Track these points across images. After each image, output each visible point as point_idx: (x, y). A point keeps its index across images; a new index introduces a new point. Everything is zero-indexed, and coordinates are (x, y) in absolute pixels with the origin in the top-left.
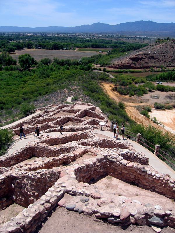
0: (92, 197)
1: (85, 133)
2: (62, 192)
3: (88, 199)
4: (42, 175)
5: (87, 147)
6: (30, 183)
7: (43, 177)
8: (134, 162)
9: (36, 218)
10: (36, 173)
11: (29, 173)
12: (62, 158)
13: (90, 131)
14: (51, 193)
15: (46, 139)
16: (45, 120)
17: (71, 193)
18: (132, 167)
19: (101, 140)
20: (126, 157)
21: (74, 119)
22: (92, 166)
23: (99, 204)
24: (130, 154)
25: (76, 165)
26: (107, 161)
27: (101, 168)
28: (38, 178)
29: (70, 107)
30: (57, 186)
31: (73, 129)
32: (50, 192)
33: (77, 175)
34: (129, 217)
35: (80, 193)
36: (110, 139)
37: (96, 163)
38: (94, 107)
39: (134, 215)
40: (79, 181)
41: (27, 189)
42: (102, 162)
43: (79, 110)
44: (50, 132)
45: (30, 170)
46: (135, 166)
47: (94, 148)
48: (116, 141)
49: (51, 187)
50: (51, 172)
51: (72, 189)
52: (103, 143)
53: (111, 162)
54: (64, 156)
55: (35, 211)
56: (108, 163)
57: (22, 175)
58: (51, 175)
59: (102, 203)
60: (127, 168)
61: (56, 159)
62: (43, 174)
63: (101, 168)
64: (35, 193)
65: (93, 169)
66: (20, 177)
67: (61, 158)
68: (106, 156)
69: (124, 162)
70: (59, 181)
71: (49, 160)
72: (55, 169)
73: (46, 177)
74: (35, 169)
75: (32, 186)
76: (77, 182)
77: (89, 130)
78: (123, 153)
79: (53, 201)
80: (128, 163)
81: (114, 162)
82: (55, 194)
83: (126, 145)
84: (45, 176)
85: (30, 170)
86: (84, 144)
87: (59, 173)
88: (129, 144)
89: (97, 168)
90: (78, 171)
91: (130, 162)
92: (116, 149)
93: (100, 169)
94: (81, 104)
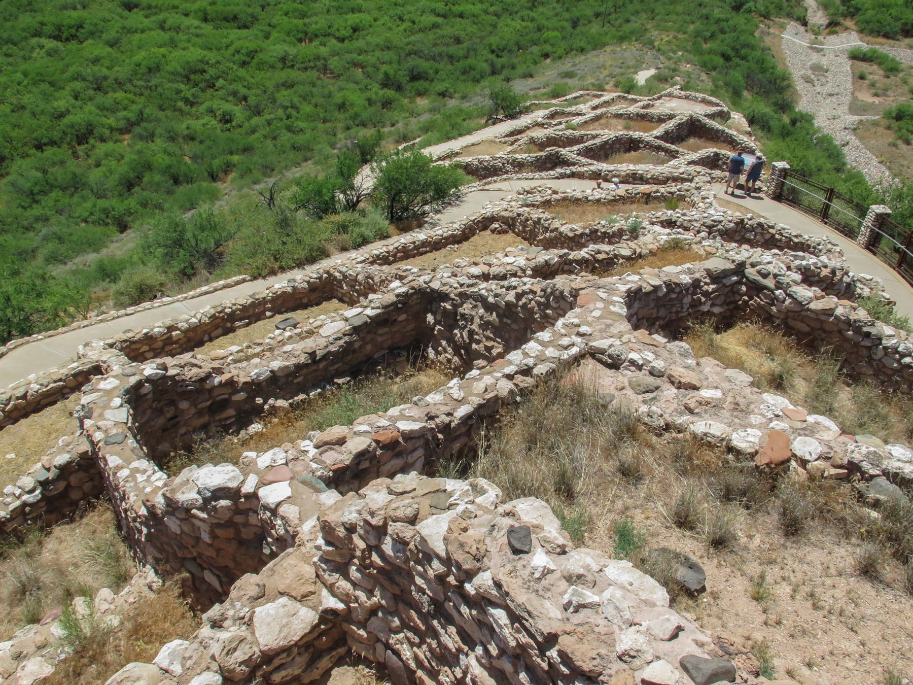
0: (672, 383)
1: (679, 191)
2: (574, 350)
3: (655, 385)
4: (519, 296)
5: (679, 233)
6: (481, 318)
7: (524, 300)
8: (839, 299)
9: (483, 412)
10: (502, 287)
11: (481, 287)
12: (590, 258)
13: (698, 188)
14: (540, 348)
15: (549, 197)
16: (551, 141)
17: (605, 358)
18: (829, 312)
19: (730, 218)
20: (809, 277)
21: (649, 146)
22: (687, 290)
23: (692, 406)
24: (828, 270)
25: (632, 280)
26: (739, 283)
27: (718, 302)
28: (508, 304)
29: (641, 104)
30: (563, 331)
31: (641, 175)
32: (536, 344)
33: (633, 311)
34: (788, 460)
35: (633, 363)
36: (762, 220)
37: (702, 284)
38: (726, 109)
39: (808, 461)
40: (636, 327)
41: (471, 333)
42: (724, 281)
43: (671, 117)
44: (562, 176)
45: (486, 277)
46: (839, 311)
47: (703, 239)
48: (784, 229)
49: (542, 329)
50: (549, 290)
51: (610, 346)
52: (736, 231)
53: (756, 288)
54: (599, 252)
55: (486, 390)
56: (744, 288)
57: (460, 290)
58: (548, 299)
59: (700, 404)
60: (812, 315)
61: (571, 257)
62: (524, 293)
63: (718, 302)
64: (492, 347)
65: (687, 300)
66: (452, 296)
67: (587, 256)
68: (742, 265)
69: (804, 293)
70: (572, 317)
71: (547, 258)
72: (561, 282)
73: (533, 302)
74: (497, 277)
75: (485, 325)
76: (630, 327)
77: (693, 185)
78: (804, 263)
79: (544, 372)
80: (817, 298)
81: (766, 288)
82: (550, 352)
83: (820, 247)
84: (530, 301)
85: (486, 277)
86: (669, 224)
87: (575, 294)
88: (829, 246)
89: (703, 299)
90: (634, 297)
91: (823, 297)
92: (780, 253)
93: (713, 305)
94: (679, 98)
